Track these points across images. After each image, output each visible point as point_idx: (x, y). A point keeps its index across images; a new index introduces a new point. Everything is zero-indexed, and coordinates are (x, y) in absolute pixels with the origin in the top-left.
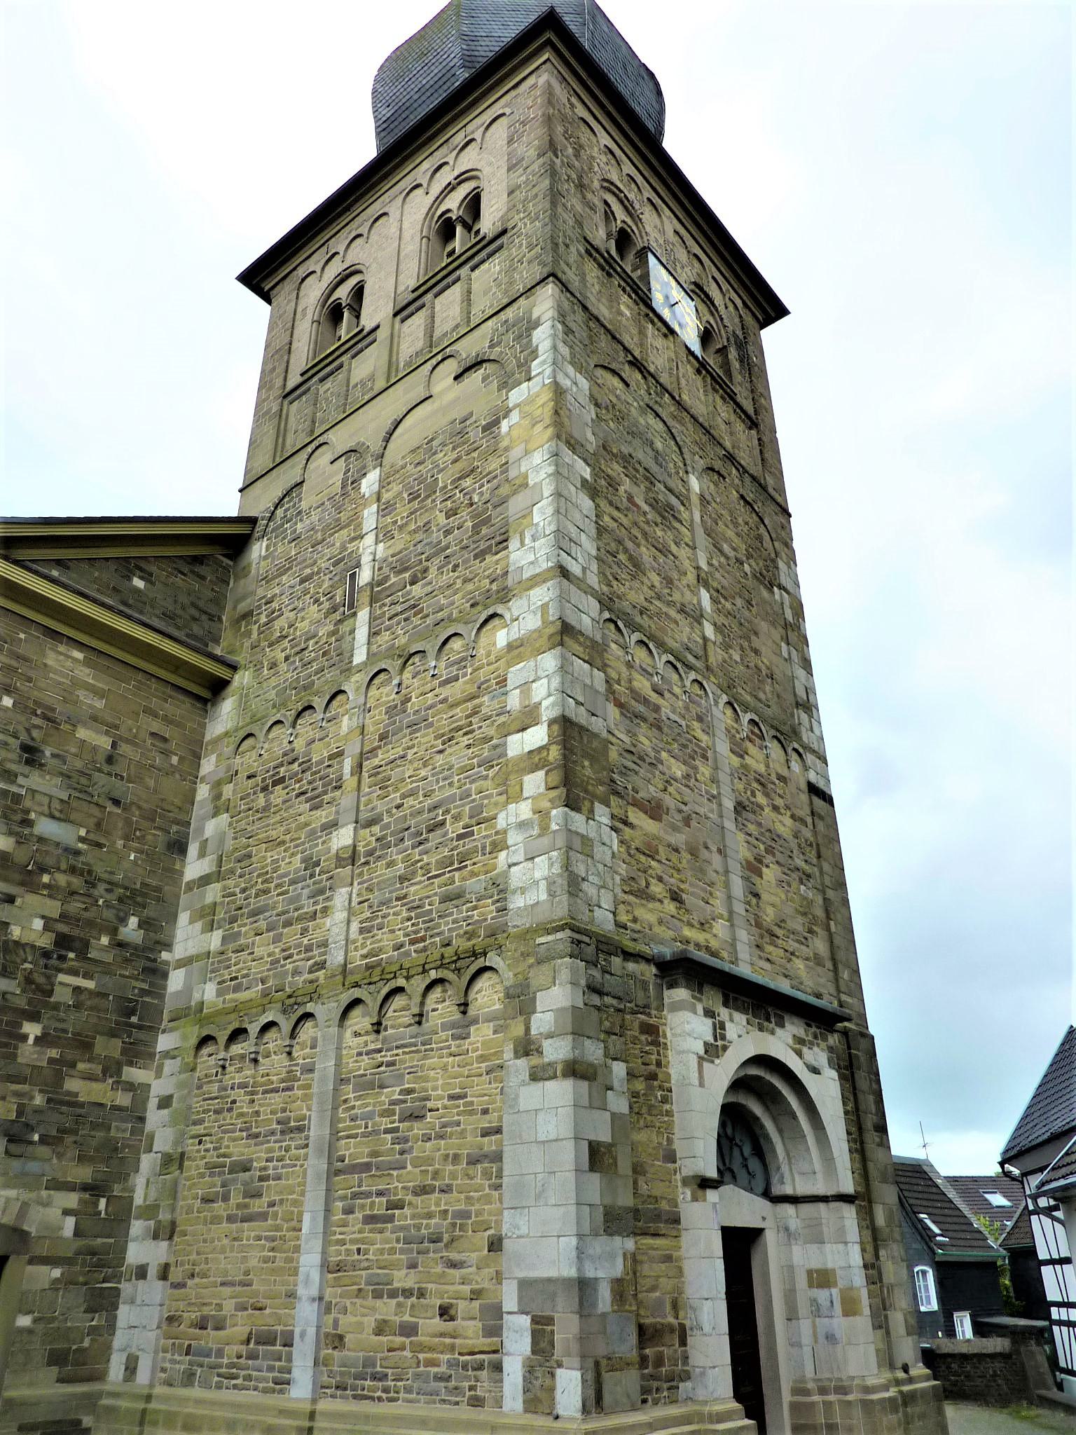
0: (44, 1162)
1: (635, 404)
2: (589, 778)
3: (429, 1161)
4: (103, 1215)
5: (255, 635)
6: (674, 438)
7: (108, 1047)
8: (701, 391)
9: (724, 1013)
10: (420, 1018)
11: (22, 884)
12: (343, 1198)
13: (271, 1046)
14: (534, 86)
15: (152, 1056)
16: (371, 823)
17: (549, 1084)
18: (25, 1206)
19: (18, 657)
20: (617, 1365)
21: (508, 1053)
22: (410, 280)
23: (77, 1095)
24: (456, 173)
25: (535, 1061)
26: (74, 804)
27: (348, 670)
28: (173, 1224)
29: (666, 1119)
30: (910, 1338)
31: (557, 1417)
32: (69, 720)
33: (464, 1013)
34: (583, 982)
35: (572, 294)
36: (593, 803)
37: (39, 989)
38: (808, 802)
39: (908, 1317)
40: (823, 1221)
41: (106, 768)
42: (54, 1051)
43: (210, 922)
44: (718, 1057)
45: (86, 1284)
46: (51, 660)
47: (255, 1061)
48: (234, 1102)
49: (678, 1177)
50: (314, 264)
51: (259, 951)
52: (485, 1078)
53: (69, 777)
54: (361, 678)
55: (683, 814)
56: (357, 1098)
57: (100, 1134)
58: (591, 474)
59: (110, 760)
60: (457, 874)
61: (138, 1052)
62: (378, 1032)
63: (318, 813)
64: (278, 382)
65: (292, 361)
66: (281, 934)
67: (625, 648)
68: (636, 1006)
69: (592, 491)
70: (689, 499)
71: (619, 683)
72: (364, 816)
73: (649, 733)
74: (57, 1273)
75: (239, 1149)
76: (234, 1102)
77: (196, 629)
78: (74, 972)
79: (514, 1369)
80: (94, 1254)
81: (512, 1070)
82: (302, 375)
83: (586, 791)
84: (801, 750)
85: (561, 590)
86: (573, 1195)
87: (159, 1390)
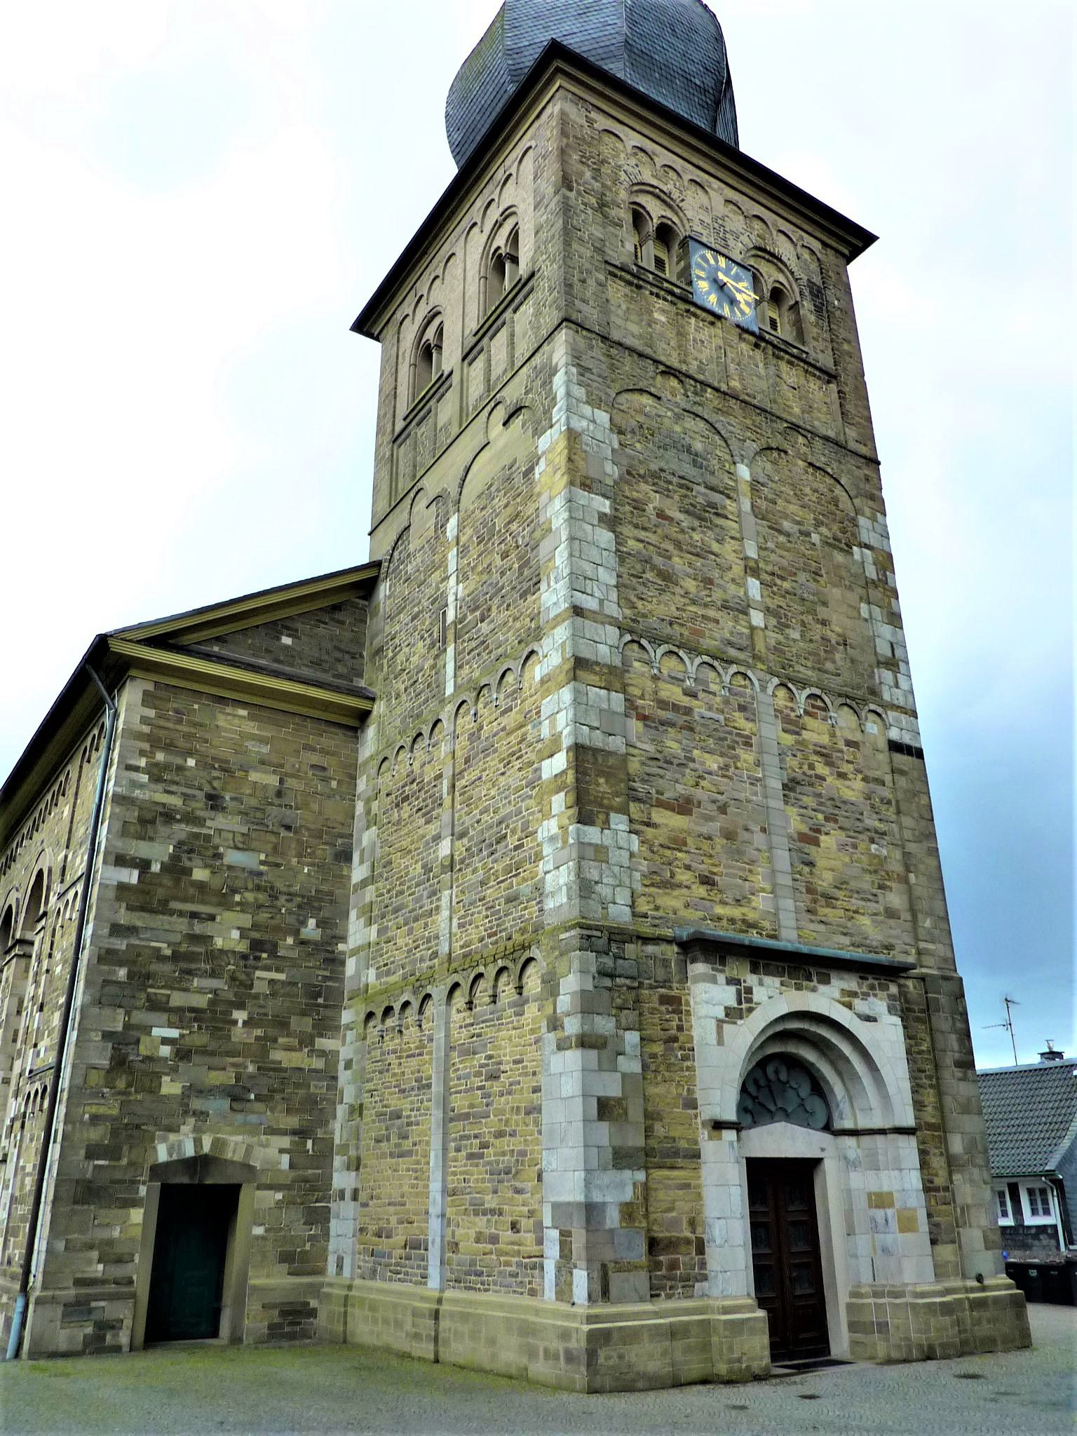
0: (261, 1114)
1: (669, 414)
2: (605, 793)
3: (502, 1112)
4: (311, 1152)
5: (385, 669)
6: (719, 433)
7: (302, 1024)
8: (761, 365)
9: (751, 979)
10: (494, 998)
11: (219, 904)
12: (455, 1140)
13: (409, 1019)
14: (551, 115)
15: (338, 1028)
16: (463, 835)
17: (568, 1053)
18: (249, 1149)
19: (195, 725)
20: (622, 1267)
21: (544, 1030)
22: (473, 325)
23: (280, 1062)
24: (501, 210)
25: (560, 1034)
26: (254, 835)
27: (442, 701)
28: (359, 1159)
29: (687, 1073)
30: (990, 1253)
31: (573, 1304)
32: (242, 769)
33: (520, 994)
34: (593, 969)
35: (588, 330)
36: (608, 815)
37: (242, 984)
38: (888, 760)
39: (989, 1233)
40: (880, 1151)
41: (277, 801)
42: (259, 1030)
43: (369, 917)
44: (741, 1018)
45: (302, 1204)
46: (222, 721)
47: (400, 1032)
48: (390, 1064)
49: (699, 1121)
50: (407, 308)
51: (400, 942)
52: (534, 1047)
53: (247, 814)
54: (450, 708)
55: (718, 804)
56: (461, 1062)
57: (302, 1092)
58: (611, 507)
59: (279, 794)
60: (514, 880)
61: (327, 1026)
62: (471, 1009)
63: (430, 826)
64: (389, 429)
65: (398, 406)
66: (412, 928)
67: (648, 663)
68: (656, 981)
69: (611, 522)
70: (735, 489)
71: (642, 697)
72: (458, 829)
73: (679, 736)
74: (279, 1196)
75: (395, 1102)
76: (390, 1064)
77: (341, 669)
78: (267, 968)
79: (550, 1266)
80: (306, 1181)
81: (546, 1042)
82: (405, 419)
83: (601, 805)
84: (880, 710)
85: (574, 628)
86: (582, 1139)
87: (358, 1282)
